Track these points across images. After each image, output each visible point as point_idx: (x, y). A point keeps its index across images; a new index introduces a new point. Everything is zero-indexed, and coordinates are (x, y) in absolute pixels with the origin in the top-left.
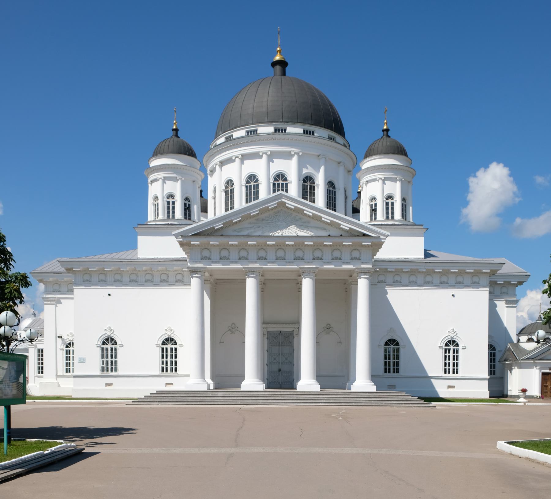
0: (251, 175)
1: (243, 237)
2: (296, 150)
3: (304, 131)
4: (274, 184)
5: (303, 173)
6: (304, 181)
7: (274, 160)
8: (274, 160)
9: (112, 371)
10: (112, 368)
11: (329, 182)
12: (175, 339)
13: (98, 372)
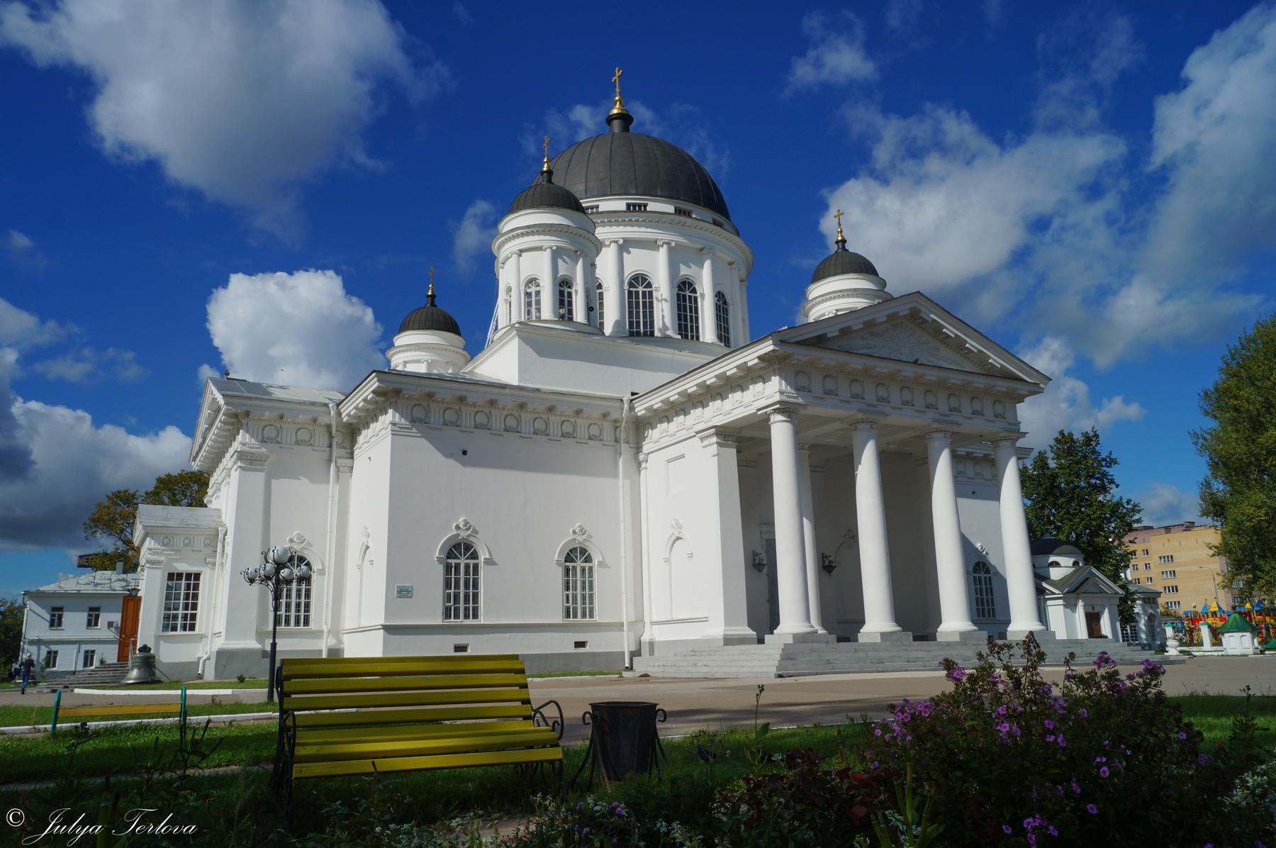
0: (639, 274)
1: (982, 376)
2: (667, 237)
3: (676, 210)
4: (630, 293)
5: (560, 274)
6: (680, 288)
7: (630, 249)
8: (630, 249)
9: (466, 616)
10: (466, 609)
11: (719, 292)
12: (308, 559)
13: (558, 619)
